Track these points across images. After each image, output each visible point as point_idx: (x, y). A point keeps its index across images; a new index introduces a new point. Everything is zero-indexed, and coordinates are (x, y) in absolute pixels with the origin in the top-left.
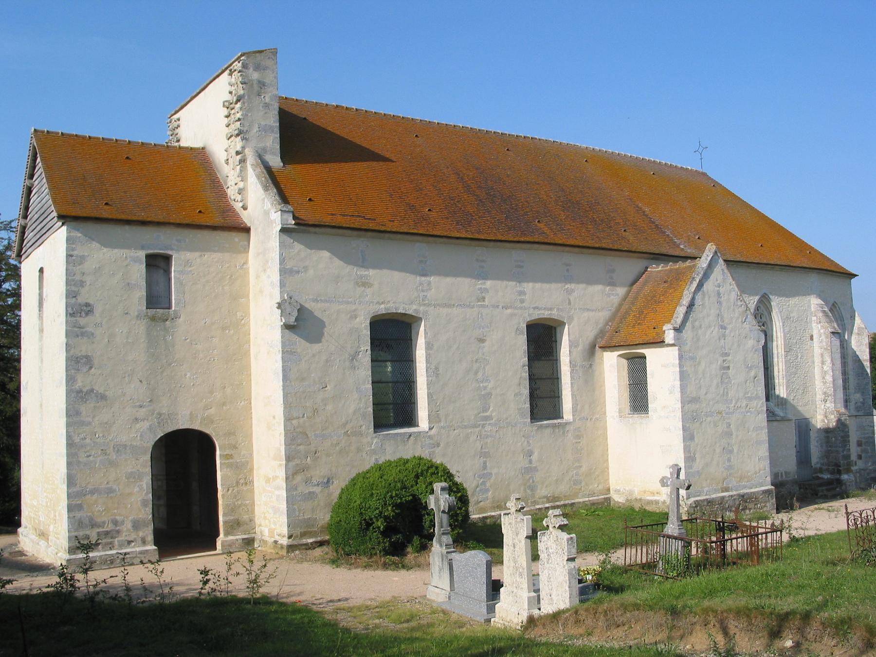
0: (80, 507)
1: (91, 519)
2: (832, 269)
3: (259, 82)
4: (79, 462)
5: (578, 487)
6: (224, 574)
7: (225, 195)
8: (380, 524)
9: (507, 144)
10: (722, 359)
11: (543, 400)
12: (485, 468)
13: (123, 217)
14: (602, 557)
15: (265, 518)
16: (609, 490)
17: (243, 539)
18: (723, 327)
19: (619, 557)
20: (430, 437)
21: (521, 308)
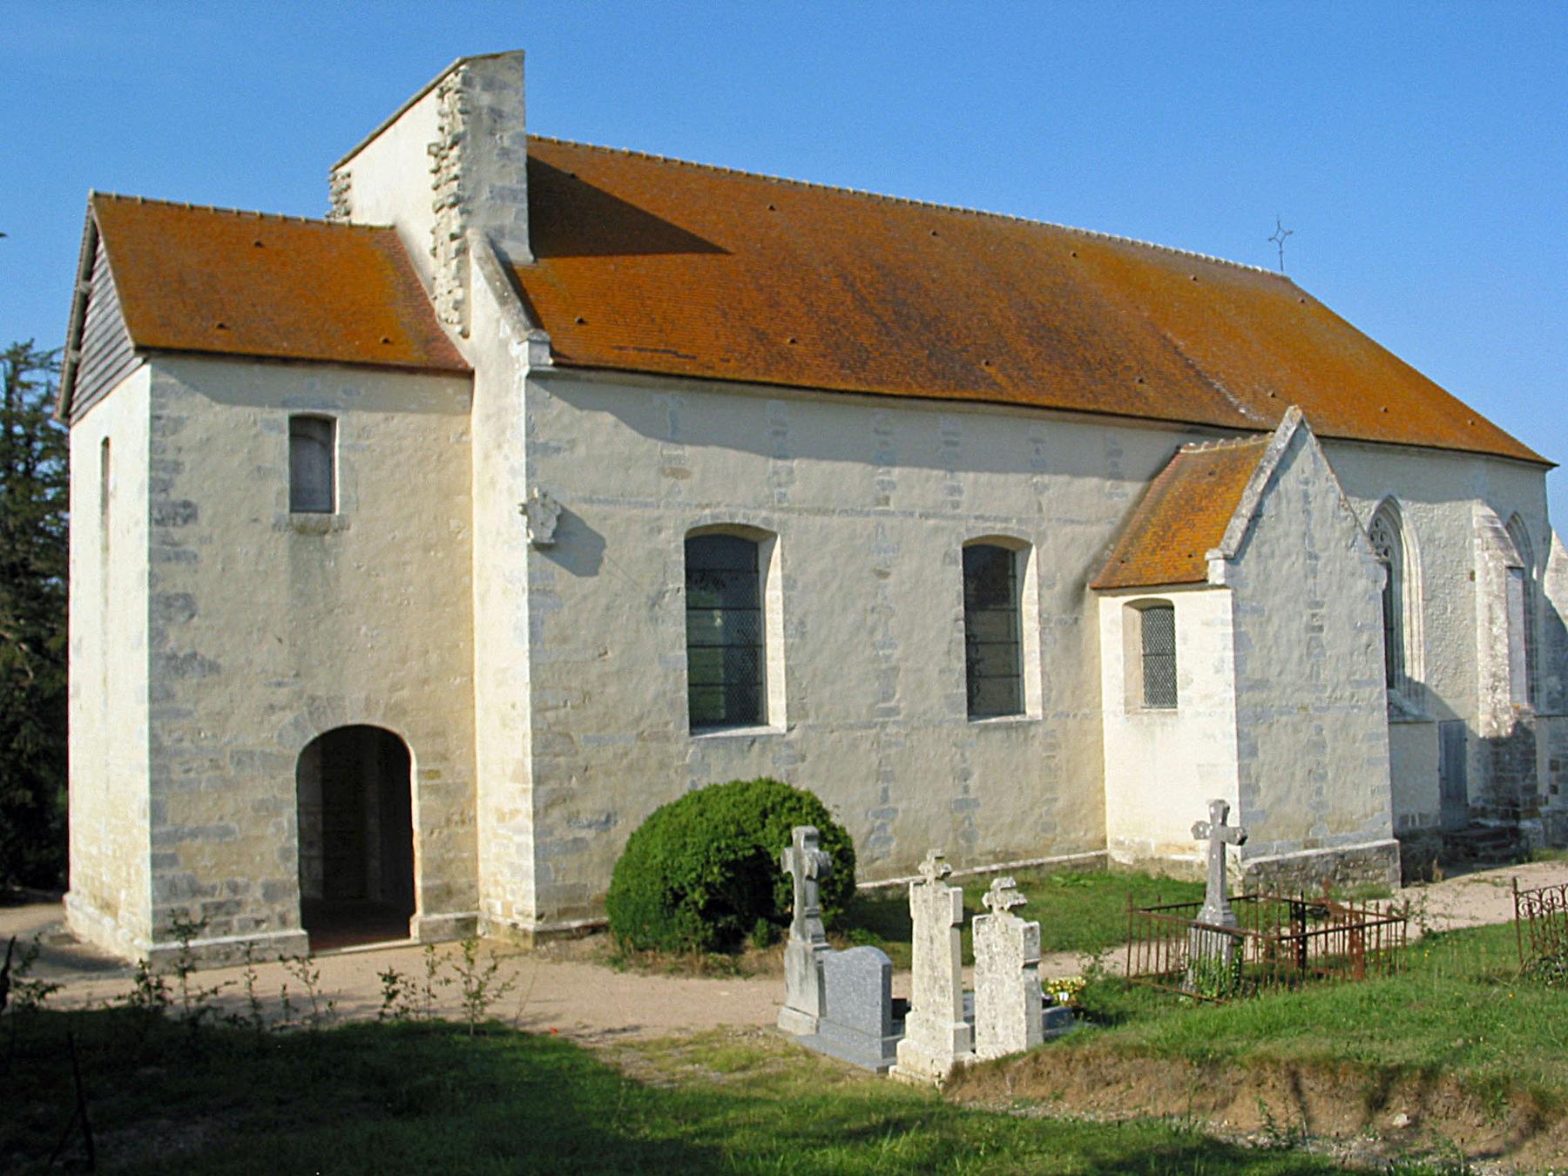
4: (170, 782)
7: (430, 311)
8: (698, 896)
11: (990, 682)
12: (885, 799)
13: (251, 349)
14: (1088, 961)
15: (496, 883)
16: (1104, 841)
17: (458, 920)
18: (1313, 556)
19: (1119, 961)
20: (789, 744)
21: (954, 517)
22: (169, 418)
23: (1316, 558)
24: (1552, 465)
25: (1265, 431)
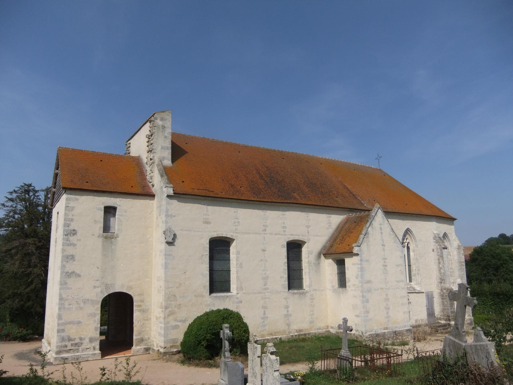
0: (63, 331)
1: (69, 337)
2: (443, 216)
3: (162, 126)
4: (64, 308)
5: (312, 325)
6: (113, 371)
7: (146, 179)
8: (204, 343)
9: (283, 155)
10: (383, 261)
11: (294, 279)
12: (264, 314)
13: (95, 189)
14: (311, 366)
15: (155, 338)
16: (328, 327)
17: (144, 348)
18: (383, 245)
19: (319, 365)
20: (237, 298)
21: (284, 235)
22: (70, 207)
23: (384, 246)
24: (455, 219)
25: (369, 211)
